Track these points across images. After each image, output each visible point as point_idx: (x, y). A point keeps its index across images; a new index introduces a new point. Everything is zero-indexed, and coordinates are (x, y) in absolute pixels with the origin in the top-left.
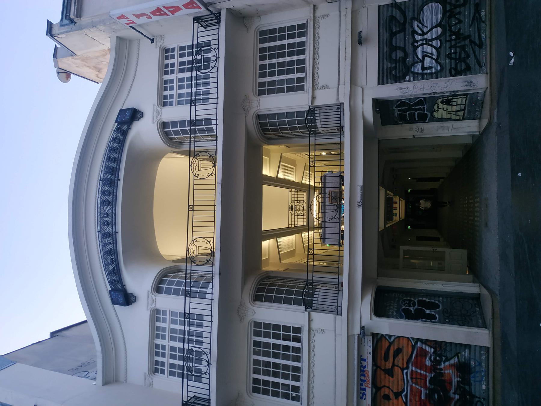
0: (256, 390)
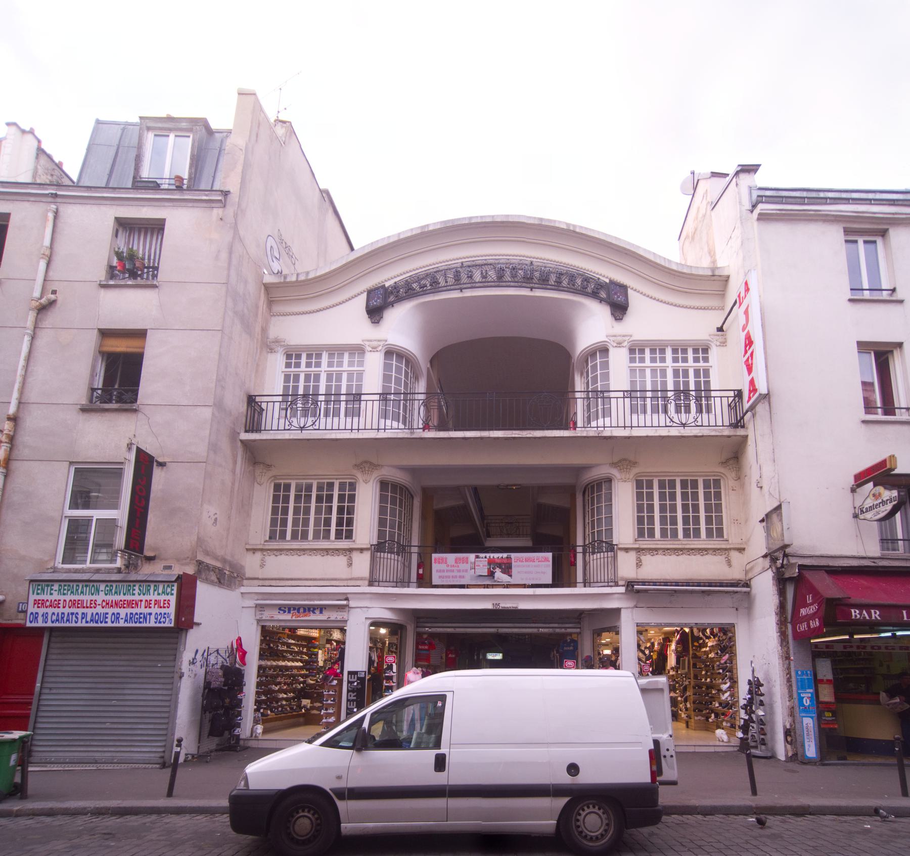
0: (277, 487)
